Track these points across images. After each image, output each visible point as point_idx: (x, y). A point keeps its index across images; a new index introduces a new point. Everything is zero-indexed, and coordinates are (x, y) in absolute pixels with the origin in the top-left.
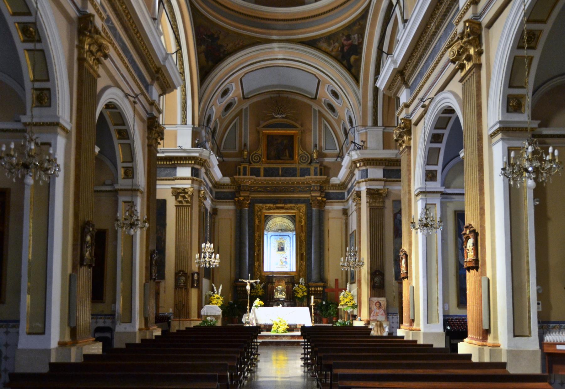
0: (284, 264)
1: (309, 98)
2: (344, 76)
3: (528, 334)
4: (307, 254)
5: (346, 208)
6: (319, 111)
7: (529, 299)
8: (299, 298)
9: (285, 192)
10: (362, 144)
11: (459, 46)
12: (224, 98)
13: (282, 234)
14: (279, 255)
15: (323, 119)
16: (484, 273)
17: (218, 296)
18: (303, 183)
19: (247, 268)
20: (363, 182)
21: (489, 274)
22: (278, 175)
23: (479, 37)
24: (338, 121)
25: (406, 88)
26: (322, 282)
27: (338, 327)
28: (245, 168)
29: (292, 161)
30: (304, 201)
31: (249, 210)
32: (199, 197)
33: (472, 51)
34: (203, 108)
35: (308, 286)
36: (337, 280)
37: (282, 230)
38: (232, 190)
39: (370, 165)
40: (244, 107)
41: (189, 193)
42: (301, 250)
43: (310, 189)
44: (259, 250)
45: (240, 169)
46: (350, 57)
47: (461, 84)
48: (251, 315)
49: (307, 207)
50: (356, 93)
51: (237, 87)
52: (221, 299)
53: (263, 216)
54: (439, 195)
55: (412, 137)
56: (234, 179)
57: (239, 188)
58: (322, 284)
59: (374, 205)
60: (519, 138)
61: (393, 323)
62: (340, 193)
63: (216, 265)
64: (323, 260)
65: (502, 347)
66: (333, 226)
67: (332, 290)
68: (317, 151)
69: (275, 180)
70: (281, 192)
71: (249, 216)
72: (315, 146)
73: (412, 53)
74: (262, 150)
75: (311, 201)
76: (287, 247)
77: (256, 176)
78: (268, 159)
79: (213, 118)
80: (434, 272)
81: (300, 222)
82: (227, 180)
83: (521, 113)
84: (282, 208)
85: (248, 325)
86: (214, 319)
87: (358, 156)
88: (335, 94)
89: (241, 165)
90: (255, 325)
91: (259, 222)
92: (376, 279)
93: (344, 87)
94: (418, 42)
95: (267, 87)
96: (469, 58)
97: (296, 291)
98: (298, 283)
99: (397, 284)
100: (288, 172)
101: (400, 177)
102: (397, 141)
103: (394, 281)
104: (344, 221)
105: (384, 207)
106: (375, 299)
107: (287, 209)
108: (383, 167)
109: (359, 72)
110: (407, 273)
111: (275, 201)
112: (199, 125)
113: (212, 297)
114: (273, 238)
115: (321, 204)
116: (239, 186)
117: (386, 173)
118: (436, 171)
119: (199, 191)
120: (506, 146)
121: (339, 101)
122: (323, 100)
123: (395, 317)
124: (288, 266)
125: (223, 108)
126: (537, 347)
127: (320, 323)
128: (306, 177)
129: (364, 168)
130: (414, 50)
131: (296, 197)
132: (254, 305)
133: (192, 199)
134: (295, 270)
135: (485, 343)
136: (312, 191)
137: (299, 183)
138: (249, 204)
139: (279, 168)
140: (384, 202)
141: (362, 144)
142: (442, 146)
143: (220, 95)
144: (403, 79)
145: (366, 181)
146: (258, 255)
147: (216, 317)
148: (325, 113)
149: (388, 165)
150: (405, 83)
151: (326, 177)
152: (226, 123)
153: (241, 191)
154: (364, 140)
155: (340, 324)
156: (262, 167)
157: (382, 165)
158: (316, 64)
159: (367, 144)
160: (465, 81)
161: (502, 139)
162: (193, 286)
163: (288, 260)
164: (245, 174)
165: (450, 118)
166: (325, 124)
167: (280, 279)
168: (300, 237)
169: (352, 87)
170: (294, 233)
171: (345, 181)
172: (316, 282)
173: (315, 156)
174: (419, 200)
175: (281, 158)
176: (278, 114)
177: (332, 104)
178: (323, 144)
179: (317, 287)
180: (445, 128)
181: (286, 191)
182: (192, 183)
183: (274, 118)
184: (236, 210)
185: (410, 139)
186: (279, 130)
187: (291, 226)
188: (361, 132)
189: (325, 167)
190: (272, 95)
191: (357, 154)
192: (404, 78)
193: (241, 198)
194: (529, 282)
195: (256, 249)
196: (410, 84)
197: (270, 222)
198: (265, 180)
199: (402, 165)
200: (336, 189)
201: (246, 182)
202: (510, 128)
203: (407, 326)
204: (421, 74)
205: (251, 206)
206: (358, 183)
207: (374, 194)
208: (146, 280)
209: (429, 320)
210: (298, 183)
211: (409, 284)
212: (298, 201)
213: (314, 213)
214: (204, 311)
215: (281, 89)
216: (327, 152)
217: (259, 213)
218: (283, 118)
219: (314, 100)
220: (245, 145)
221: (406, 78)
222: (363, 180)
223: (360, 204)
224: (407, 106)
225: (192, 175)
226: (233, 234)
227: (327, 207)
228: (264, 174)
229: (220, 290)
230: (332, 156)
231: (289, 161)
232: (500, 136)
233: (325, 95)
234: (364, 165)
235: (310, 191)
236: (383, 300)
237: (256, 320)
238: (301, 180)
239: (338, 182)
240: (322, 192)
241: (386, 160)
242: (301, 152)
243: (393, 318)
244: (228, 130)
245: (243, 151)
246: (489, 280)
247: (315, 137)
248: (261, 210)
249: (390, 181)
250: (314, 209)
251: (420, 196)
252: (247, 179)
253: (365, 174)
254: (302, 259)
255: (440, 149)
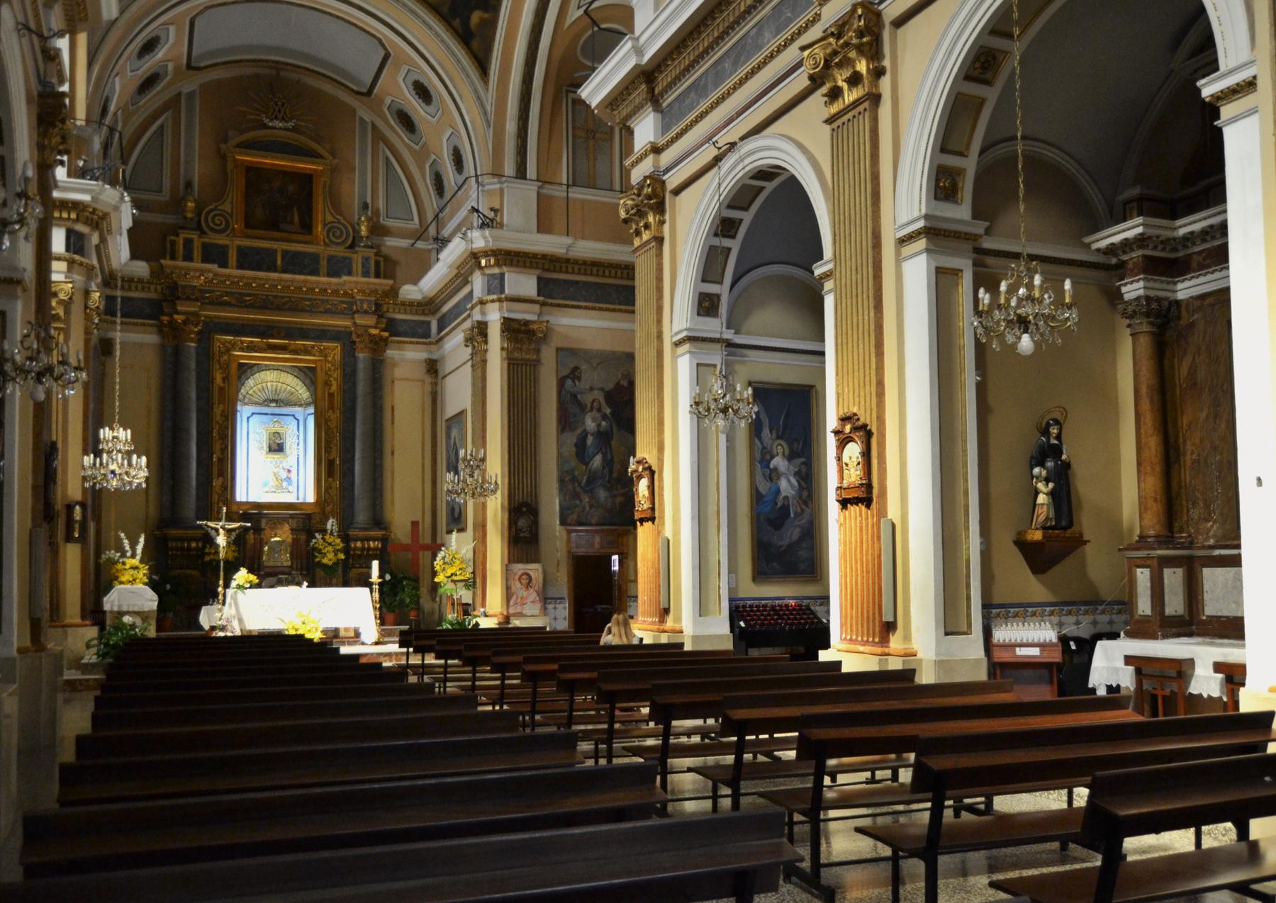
0: (285, 484)
1: (353, 90)
2: (453, 54)
3: (965, 629)
4: (343, 462)
5: (434, 357)
6: (374, 126)
7: (968, 561)
8: (326, 566)
9: (290, 309)
10: (491, 215)
11: (828, 51)
12: (143, 61)
13: (277, 411)
14: (274, 463)
15: (382, 145)
16: (882, 513)
17: (135, 562)
18: (335, 292)
19: (194, 492)
20: (493, 301)
21: (893, 513)
22: (273, 268)
23: (877, 40)
24: (421, 156)
25: (655, 110)
26: (381, 529)
27: (447, 630)
28: (188, 243)
29: (307, 238)
30: (335, 335)
31: (197, 348)
32: (86, 307)
33: (862, 66)
34: (99, 78)
35: (346, 539)
36: (415, 524)
37: (278, 402)
38: (153, 296)
39: (511, 264)
40: (186, 90)
41: (62, 296)
42: (328, 450)
43: (351, 309)
44: (224, 450)
45: (173, 243)
46: (471, 13)
47: (828, 128)
48: (228, 611)
49: (343, 349)
50: (479, 98)
51: (178, 35)
52: (144, 569)
53: (234, 367)
54: (718, 346)
55: (667, 217)
56: (162, 267)
57: (173, 292)
58: (379, 533)
59: (516, 355)
60: (954, 253)
61: (555, 619)
62: (426, 321)
63: (140, 484)
64: (381, 476)
65: (920, 655)
66: (405, 399)
67: (405, 548)
68: (369, 220)
69: (267, 280)
70: (279, 309)
71: (198, 363)
72: (365, 206)
73: (684, 40)
74: (232, 204)
75: (354, 338)
76: (290, 443)
77: (220, 266)
78: (247, 225)
79: (112, 108)
80: (712, 509)
81: (327, 384)
82: (141, 269)
83: (956, 202)
84: (283, 348)
85: (221, 634)
86: (138, 621)
87: (487, 242)
88: (423, 92)
89: (177, 235)
90: (238, 633)
91: (224, 379)
92: (522, 522)
93: (451, 79)
94: (705, 19)
95: (251, 48)
96: (855, 80)
97: (320, 551)
98: (324, 531)
99: (564, 534)
100: (296, 263)
101: (632, 303)
102: (626, 221)
103: (558, 527)
104: (428, 388)
105: (537, 362)
106: (519, 568)
107: (295, 352)
108: (538, 272)
109: (488, 50)
110: (653, 509)
111: (264, 331)
112: (88, 121)
113: (119, 566)
114: (254, 420)
115: (378, 346)
116: (174, 287)
117: (543, 285)
118: (718, 296)
119: (87, 293)
120: (934, 265)
121: (431, 109)
122: (388, 101)
123: (560, 606)
124: (293, 488)
125: (135, 84)
126: (980, 653)
127: (189, 629)
128: (345, 278)
129: (496, 271)
130: (691, 33)
131: (318, 325)
132: (234, 584)
133: (67, 312)
134: (311, 498)
135: (886, 650)
136: (357, 311)
137: (326, 290)
138: (199, 333)
139: (275, 251)
140: (538, 351)
141: (491, 215)
142: (735, 245)
143: (137, 50)
144: (651, 90)
145: (500, 300)
146: (222, 461)
147: (143, 615)
148: (388, 133)
149: (548, 270)
150: (655, 101)
151: (391, 282)
152: (137, 121)
153: (178, 298)
154: (497, 207)
155: (452, 624)
156: (234, 244)
157: (537, 268)
158: (383, 12)
159: (502, 217)
160: (839, 122)
161: (928, 250)
162: (69, 538)
163: (293, 475)
164: (188, 257)
165: (762, 188)
166: (387, 158)
167: (276, 522)
168: (326, 421)
169: (472, 83)
170: (311, 410)
171: (437, 295)
172: (366, 529)
173: (364, 230)
174: (682, 355)
175: (281, 226)
176: (276, 118)
177: (411, 113)
178: (381, 204)
179: (368, 539)
180: (746, 209)
181: (294, 308)
182: (70, 270)
183: (265, 127)
184: (162, 347)
185: (662, 222)
186: (277, 158)
187: (303, 393)
188: (487, 187)
189: (386, 258)
190: (260, 71)
191: (485, 238)
192: (653, 89)
193: (179, 318)
194: (967, 528)
195: (217, 447)
196: (664, 105)
197: (251, 382)
198: (241, 278)
199: (637, 276)
200: (411, 313)
201: (194, 277)
202: (940, 230)
203: (653, 623)
204: (699, 89)
205: (205, 337)
206: (482, 303)
207: (519, 331)
208: (33, 520)
209: (702, 609)
210: (324, 291)
211: (659, 533)
212: (322, 334)
213: (361, 366)
214: (111, 602)
215: (282, 59)
216: (390, 223)
217: (226, 357)
218: (286, 129)
219: (363, 98)
220: (189, 185)
221: (657, 91)
222: (495, 297)
223: (486, 351)
224: (656, 150)
225: (68, 249)
226: (154, 405)
227: (391, 353)
228: (238, 260)
229: (139, 548)
230: (403, 234)
231: (301, 237)
232: (922, 243)
233: (397, 89)
234: (497, 264)
235: (351, 312)
236: (535, 569)
237: (241, 621)
238: (329, 284)
239: (418, 297)
240: (380, 316)
241: (544, 256)
242: (329, 218)
243: (555, 608)
244: (142, 142)
245: (184, 199)
246: (893, 526)
247: (360, 185)
248: (228, 350)
249: (552, 305)
250: (361, 356)
251: (686, 347)
252: (196, 270)
253: (496, 285)
254: (330, 473)
255: (729, 249)
